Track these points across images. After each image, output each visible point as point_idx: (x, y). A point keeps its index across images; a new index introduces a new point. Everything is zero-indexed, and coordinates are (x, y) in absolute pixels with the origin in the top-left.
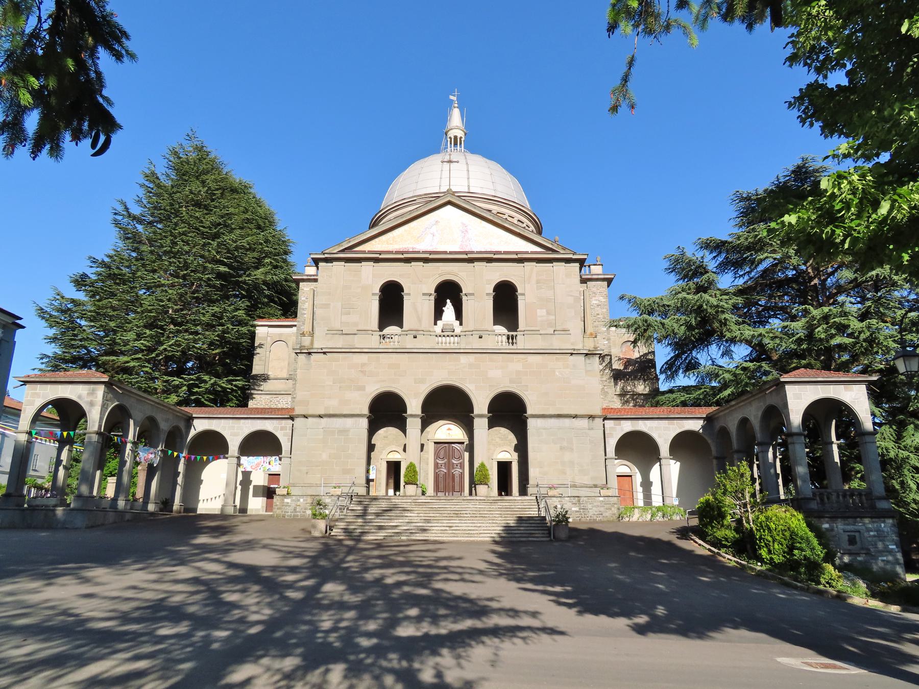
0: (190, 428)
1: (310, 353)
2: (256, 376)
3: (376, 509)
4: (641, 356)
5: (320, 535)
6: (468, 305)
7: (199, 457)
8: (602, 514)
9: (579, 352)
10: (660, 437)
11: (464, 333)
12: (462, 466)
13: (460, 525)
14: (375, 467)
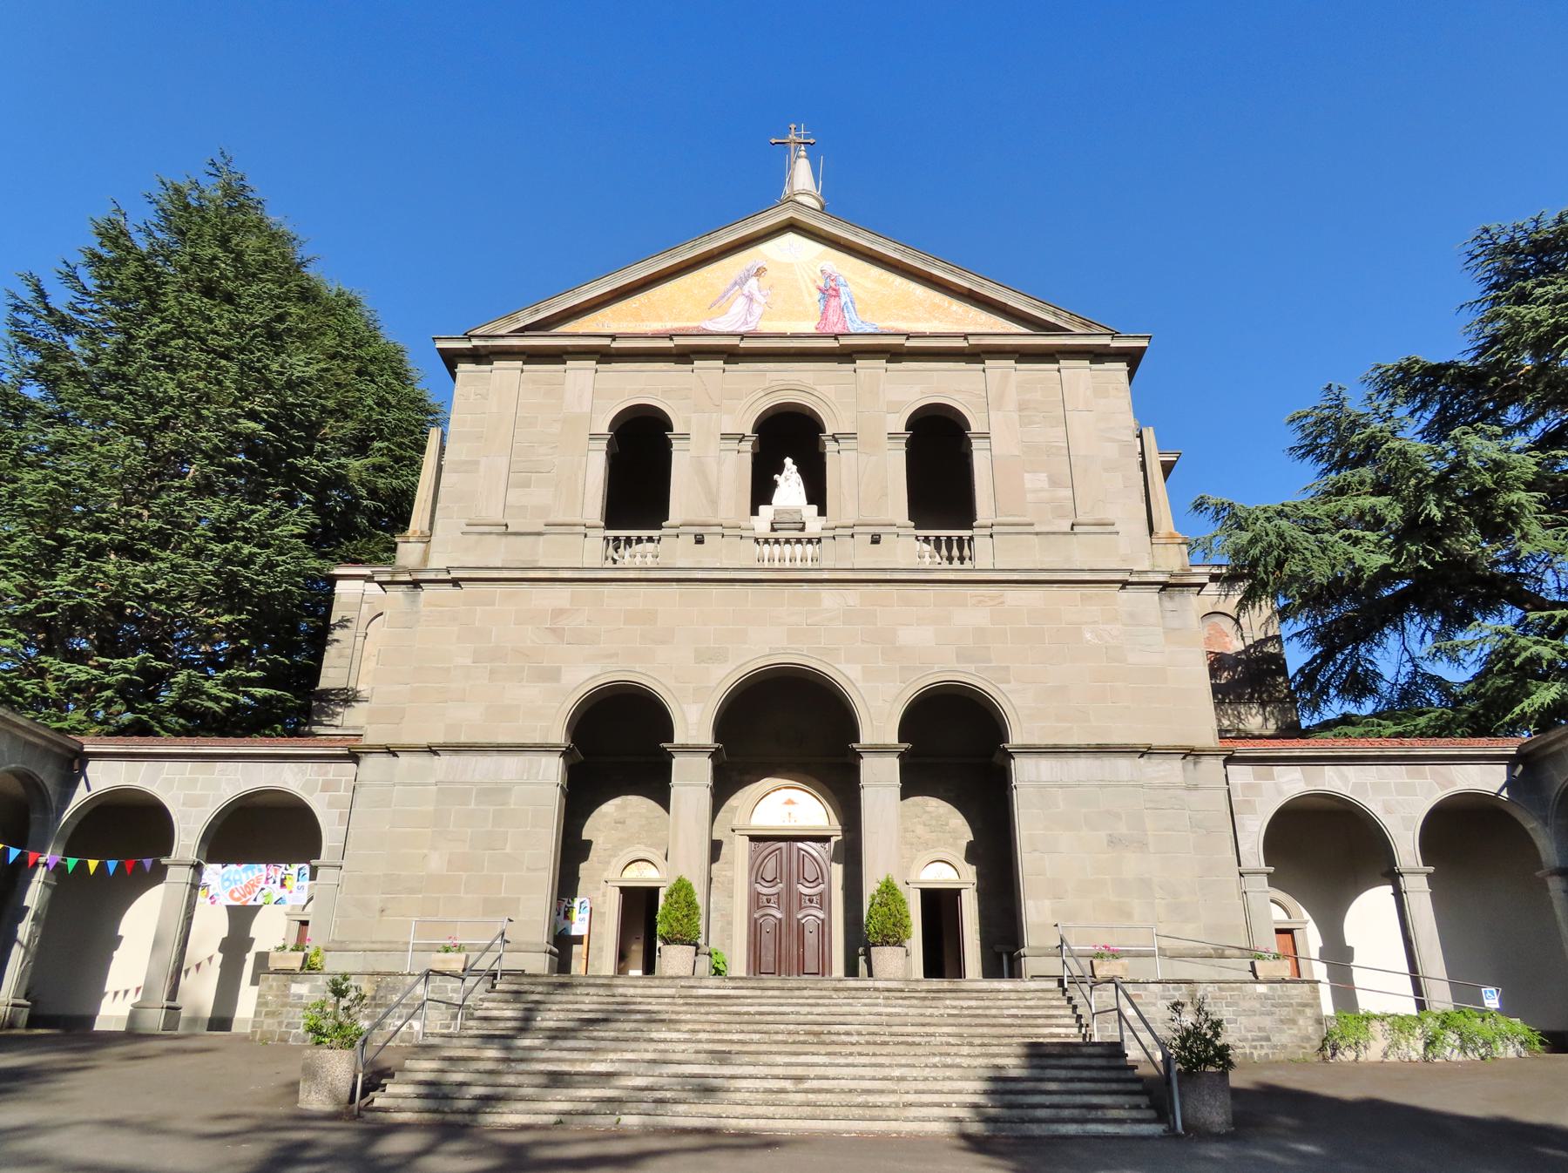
0: (75, 785)
1: (416, 584)
2: (327, 692)
3: (562, 1016)
4: (1248, 648)
5: (329, 1107)
6: (839, 465)
7: (93, 864)
8: (1268, 1039)
9: (1144, 578)
10: (1388, 811)
11: (831, 533)
12: (824, 901)
13: (831, 1072)
14: (587, 904)
